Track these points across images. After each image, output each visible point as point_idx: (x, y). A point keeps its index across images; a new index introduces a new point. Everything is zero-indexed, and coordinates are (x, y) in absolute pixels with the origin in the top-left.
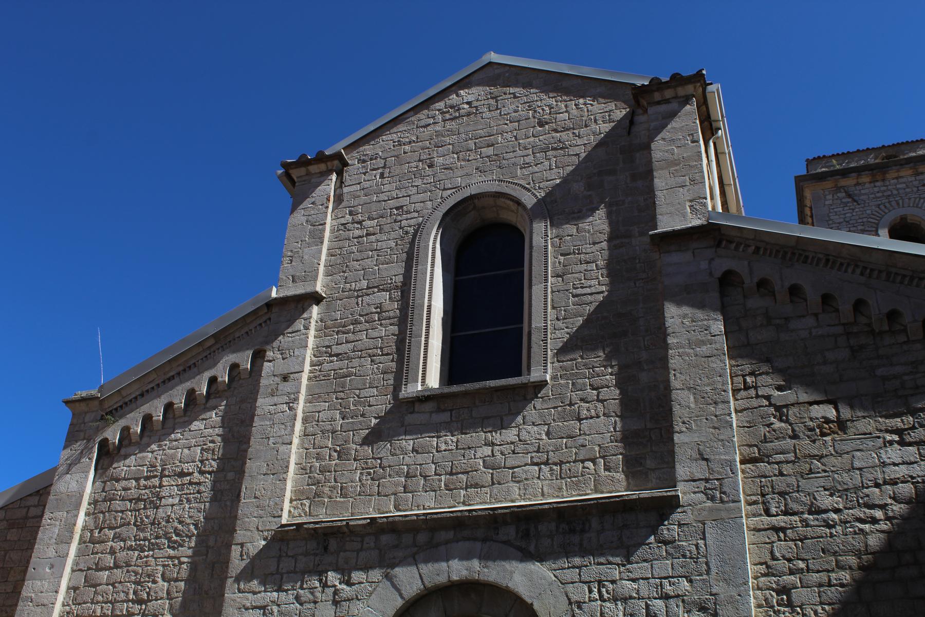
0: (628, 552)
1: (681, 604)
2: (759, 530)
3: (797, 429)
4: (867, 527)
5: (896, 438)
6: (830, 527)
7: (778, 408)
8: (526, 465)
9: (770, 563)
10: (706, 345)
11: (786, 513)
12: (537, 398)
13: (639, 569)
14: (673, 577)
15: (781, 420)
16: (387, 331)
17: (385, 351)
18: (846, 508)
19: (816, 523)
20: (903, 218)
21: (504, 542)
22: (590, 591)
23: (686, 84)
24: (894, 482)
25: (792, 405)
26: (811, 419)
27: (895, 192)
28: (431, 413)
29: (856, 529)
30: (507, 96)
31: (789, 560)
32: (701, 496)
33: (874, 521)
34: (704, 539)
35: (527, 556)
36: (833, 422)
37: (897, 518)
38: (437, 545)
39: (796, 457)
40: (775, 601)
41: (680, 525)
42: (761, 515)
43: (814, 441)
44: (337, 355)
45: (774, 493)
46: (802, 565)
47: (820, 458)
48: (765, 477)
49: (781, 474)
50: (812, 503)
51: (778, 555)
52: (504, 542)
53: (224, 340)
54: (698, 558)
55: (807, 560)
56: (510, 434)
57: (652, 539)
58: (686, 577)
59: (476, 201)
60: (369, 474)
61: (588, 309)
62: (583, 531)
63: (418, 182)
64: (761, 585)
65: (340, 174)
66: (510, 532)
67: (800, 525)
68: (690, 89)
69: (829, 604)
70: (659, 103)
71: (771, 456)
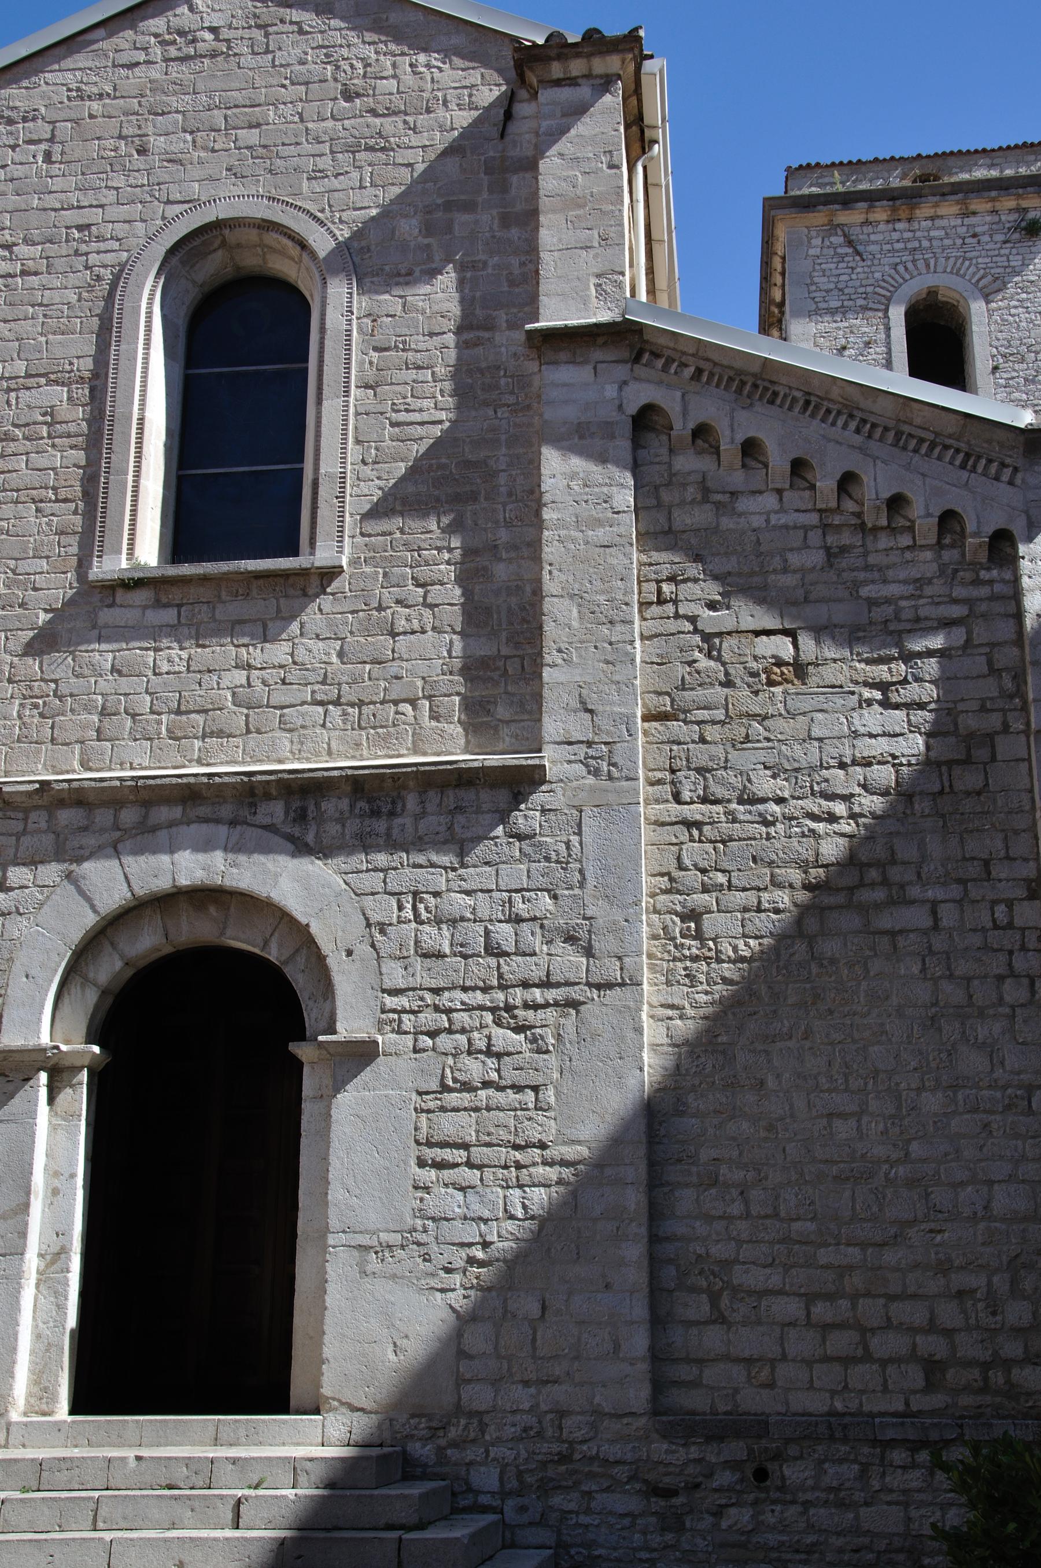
0: (462, 849)
1: (538, 930)
2: (663, 824)
3: (732, 671)
4: (820, 827)
5: (878, 695)
6: (766, 823)
7: (707, 637)
9: (676, 874)
10: (603, 526)
11: (704, 800)
12: (325, 593)
13: (477, 876)
14: (528, 890)
15: (709, 656)
18: (793, 797)
19: (748, 817)
20: (932, 292)
21: (265, 827)
22: (400, 908)
23: (609, 52)
25: (729, 633)
26: (755, 658)
27: (925, 244)
29: (806, 829)
31: (704, 871)
32: (580, 769)
33: (832, 818)
34: (579, 833)
35: (301, 848)
36: (788, 664)
39: (727, 715)
40: (677, 930)
41: (544, 811)
42: (667, 801)
43: (756, 693)
46: (721, 878)
49: (703, 740)
51: (687, 862)
52: (265, 827)
54: (568, 863)
56: (279, 652)
57: (500, 830)
58: (548, 891)
60: (36, 706)
62: (392, 814)
67: (723, 818)
69: (756, 937)
70: (558, 83)
71: (689, 711)
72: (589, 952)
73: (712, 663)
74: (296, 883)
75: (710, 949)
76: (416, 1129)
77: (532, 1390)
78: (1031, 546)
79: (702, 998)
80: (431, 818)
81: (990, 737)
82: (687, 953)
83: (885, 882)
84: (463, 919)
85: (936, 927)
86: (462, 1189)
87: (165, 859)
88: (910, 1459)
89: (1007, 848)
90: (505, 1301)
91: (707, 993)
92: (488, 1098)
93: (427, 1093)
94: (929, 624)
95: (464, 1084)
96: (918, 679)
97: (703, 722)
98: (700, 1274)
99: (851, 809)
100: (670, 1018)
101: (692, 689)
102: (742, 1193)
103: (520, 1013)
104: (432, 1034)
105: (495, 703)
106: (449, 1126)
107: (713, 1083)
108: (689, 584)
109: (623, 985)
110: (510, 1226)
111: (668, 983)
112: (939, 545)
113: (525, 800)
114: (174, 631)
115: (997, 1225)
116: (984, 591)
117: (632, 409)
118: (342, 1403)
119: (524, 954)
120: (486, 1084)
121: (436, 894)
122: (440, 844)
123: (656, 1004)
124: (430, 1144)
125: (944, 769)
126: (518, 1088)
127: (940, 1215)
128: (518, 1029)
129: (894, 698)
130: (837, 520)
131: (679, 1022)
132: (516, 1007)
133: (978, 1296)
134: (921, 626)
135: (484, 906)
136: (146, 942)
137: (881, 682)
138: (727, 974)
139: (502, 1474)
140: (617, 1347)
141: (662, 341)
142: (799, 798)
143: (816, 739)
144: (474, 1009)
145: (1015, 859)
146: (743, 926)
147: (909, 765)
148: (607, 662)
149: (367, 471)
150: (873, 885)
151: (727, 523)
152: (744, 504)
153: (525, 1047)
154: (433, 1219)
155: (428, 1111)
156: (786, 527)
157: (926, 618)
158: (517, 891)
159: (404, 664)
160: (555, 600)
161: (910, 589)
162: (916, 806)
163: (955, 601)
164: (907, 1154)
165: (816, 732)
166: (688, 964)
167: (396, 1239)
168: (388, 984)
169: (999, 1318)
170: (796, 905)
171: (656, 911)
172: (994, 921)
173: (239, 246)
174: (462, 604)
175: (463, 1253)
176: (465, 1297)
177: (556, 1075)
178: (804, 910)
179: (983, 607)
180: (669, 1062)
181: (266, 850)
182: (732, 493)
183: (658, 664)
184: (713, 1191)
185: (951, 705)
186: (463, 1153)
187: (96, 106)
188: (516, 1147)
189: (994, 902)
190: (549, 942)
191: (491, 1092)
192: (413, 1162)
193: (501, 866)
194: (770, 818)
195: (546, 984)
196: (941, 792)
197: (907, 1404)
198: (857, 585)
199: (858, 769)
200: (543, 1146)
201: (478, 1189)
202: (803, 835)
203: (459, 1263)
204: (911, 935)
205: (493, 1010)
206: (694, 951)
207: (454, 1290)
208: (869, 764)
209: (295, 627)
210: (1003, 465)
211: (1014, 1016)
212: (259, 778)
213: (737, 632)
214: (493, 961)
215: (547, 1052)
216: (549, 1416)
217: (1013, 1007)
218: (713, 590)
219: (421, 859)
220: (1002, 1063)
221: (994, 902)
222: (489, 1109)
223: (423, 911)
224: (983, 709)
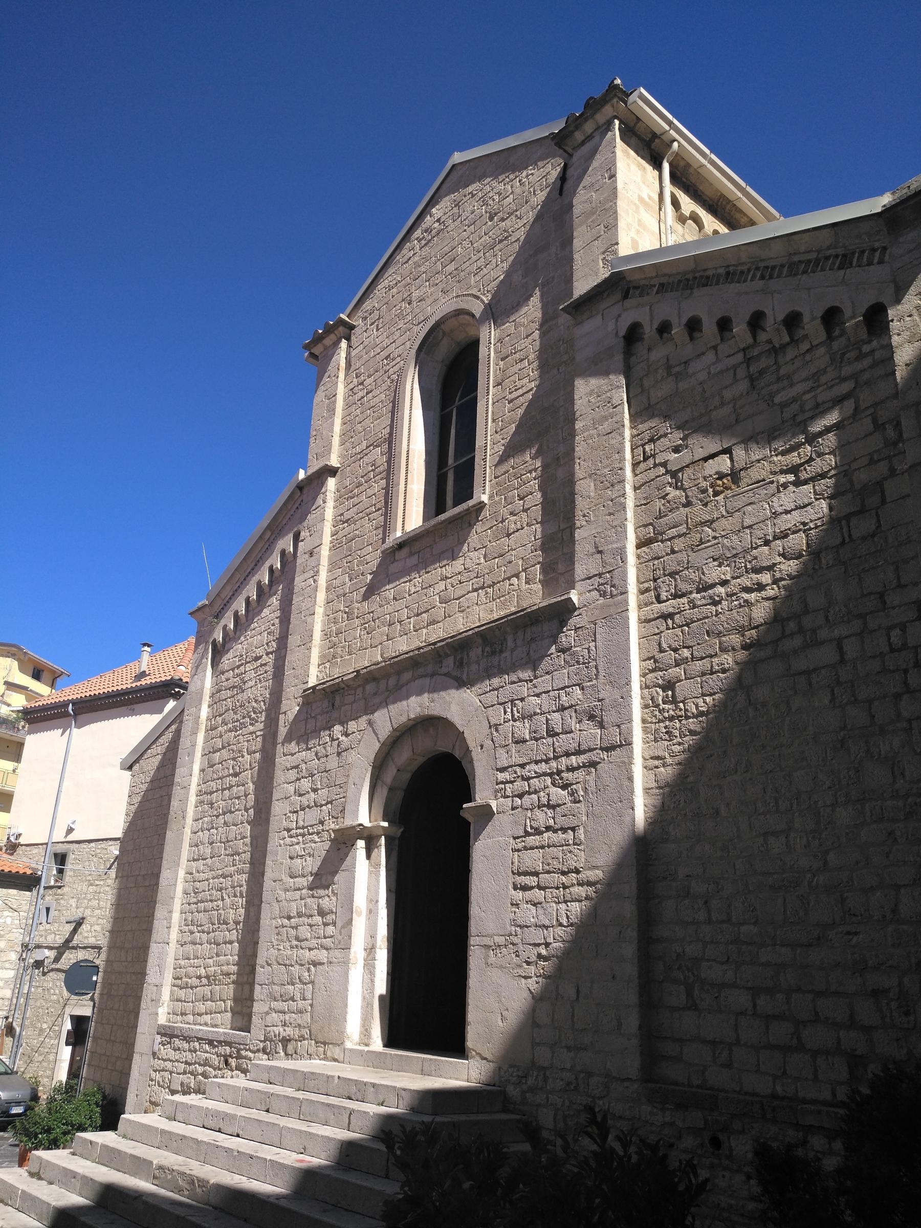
0: (534, 666)
1: (573, 714)
2: (649, 621)
3: (690, 494)
4: (752, 597)
5: (791, 478)
6: (715, 603)
7: (674, 474)
8: (469, 592)
9: (658, 656)
10: (607, 420)
11: (676, 596)
12: (478, 521)
13: (544, 683)
14: (568, 687)
15: (677, 488)
16: (377, 487)
17: (378, 506)
18: (733, 578)
19: (704, 602)
21: (445, 675)
22: (505, 713)
23: (602, 106)
24: (784, 535)
25: (687, 466)
26: (705, 478)
28: (405, 558)
29: (742, 601)
30: (468, 197)
31: (675, 650)
32: (595, 594)
33: (761, 587)
34: (595, 641)
35: (461, 683)
36: (727, 475)
37: (785, 579)
38: (402, 686)
39: (688, 528)
40: (660, 698)
41: (576, 629)
42: (652, 603)
43: (706, 505)
44: (347, 521)
45: (665, 575)
46: (686, 653)
47: (710, 523)
48: (658, 558)
49: (673, 552)
50: (700, 579)
51: (664, 645)
52: (445, 675)
53: (275, 529)
54: (589, 663)
55: (692, 647)
56: (458, 565)
57: (553, 649)
58: (578, 685)
59: (442, 326)
60: (365, 628)
61: (520, 412)
62: (501, 652)
63: (401, 324)
64: (648, 682)
65: (348, 339)
66: (449, 663)
67: (687, 607)
68: (608, 110)
69: (711, 695)
70: (583, 143)
71: (664, 533)
72: (602, 726)
73: (678, 492)
74: (461, 706)
75: (681, 710)
76: (512, 863)
77: (572, 1054)
78: (899, 307)
79: (675, 749)
80: (519, 649)
81: (880, 483)
82: (666, 715)
83: (801, 630)
84: (535, 714)
85: (842, 661)
86: (535, 905)
87: (404, 703)
88: (827, 1146)
89: (899, 578)
90: (557, 987)
91: (680, 744)
92: (549, 838)
93: (518, 838)
94: (826, 406)
95: (536, 829)
96: (820, 455)
97: (673, 538)
98: (678, 969)
99: (774, 575)
100: (657, 767)
101: (665, 516)
102: (706, 903)
103: (564, 775)
104: (520, 796)
105: (557, 563)
106: (534, 859)
107: (685, 815)
108: (662, 440)
109: (621, 746)
110: (559, 931)
111: (656, 740)
112: (830, 337)
113: (566, 625)
114: (417, 568)
115: (905, 927)
116: (867, 362)
117: (622, 332)
118: (478, 1054)
119: (567, 733)
120: (548, 828)
121: (522, 700)
122: (523, 666)
123: (648, 757)
124: (519, 874)
125: (844, 522)
126: (564, 830)
127: (854, 919)
128: (564, 787)
129: (803, 476)
130: (756, 352)
131: (662, 769)
132: (563, 771)
133: (891, 995)
134: (820, 410)
135: (546, 702)
136: (404, 756)
137: (793, 466)
138: (692, 727)
139: (555, 1115)
140: (620, 1025)
141: (637, 276)
142: (738, 577)
143: (747, 527)
144: (541, 775)
145: (906, 586)
146: (702, 687)
147: (816, 527)
148: (610, 514)
149: (498, 437)
150: (792, 634)
151: (683, 385)
152: (694, 367)
153: (568, 799)
154: (520, 926)
155: (518, 850)
156: (721, 372)
157: (824, 402)
158: (562, 689)
159: (513, 553)
160: (582, 481)
161: (810, 383)
162: (823, 561)
163: (844, 380)
164: (826, 863)
165: (748, 522)
166: (667, 723)
167: (501, 940)
168: (499, 765)
169: (912, 1018)
170: (737, 663)
171: (647, 687)
172: (890, 644)
173: (452, 331)
174: (541, 503)
175: (535, 951)
176: (537, 983)
177: (584, 818)
178: (744, 666)
179: (866, 376)
180: (657, 801)
181: (445, 688)
182: (685, 363)
183: (645, 504)
184: (686, 902)
185: (846, 468)
186: (536, 879)
187: (395, 290)
188: (564, 873)
189: (890, 628)
190: (580, 722)
191: (550, 834)
192: (511, 887)
193: (555, 673)
194: (717, 598)
195: (578, 752)
196: (843, 543)
197: (834, 1095)
198: (772, 396)
199: (777, 542)
200: (577, 871)
201: (544, 905)
202: (741, 606)
203: (533, 958)
204: (823, 672)
205: (551, 775)
206: (671, 712)
207: (531, 977)
208: (786, 536)
209: (465, 548)
210: (874, 250)
211: (911, 729)
212: (439, 644)
213: (693, 463)
214: (550, 740)
215: (579, 801)
216: (582, 1075)
217: (909, 721)
218: (676, 437)
219: (514, 677)
220: (903, 774)
221: (890, 628)
222: (549, 846)
223: (515, 712)
224: (872, 462)
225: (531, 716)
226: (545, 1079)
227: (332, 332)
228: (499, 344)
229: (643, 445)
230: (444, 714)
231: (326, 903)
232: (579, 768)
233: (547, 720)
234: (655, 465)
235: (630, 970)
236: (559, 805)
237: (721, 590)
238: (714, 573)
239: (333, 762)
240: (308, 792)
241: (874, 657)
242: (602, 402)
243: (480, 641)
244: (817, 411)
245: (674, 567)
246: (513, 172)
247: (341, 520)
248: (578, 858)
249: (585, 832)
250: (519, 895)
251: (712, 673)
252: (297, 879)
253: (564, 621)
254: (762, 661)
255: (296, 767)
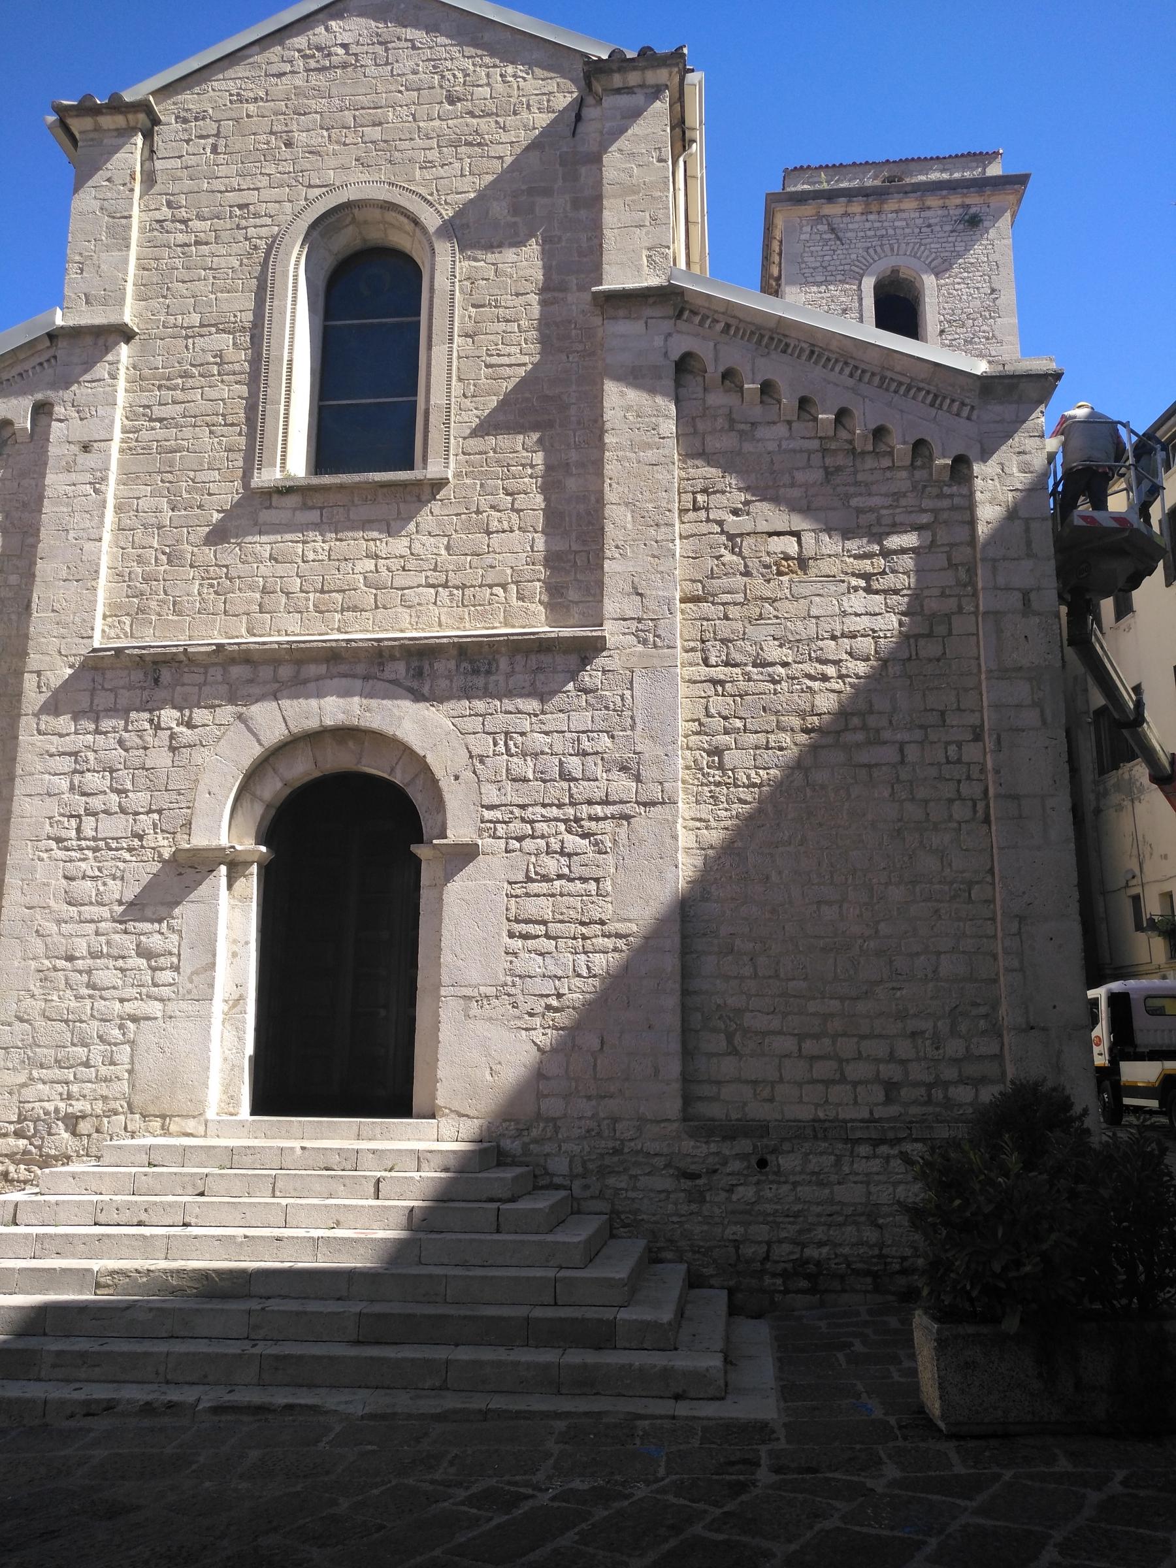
1: (600, 762)
2: (695, 682)
3: (750, 564)
4: (816, 685)
5: (862, 583)
6: (774, 682)
7: (731, 537)
8: (419, 586)
9: (704, 720)
11: (727, 664)
12: (435, 499)
13: (554, 721)
14: (592, 732)
15: (733, 553)
18: (795, 662)
19: (761, 677)
22: (495, 744)
23: (659, 66)
24: (853, 636)
25: (748, 534)
28: (295, 509)
31: (725, 718)
33: (825, 678)
34: (631, 689)
36: (793, 558)
41: (604, 672)
43: (768, 581)
44: (160, 420)
45: (716, 640)
46: (739, 724)
49: (726, 618)
51: (713, 711)
52: (390, 682)
56: (399, 545)
57: (570, 686)
58: (607, 732)
60: (212, 586)
67: (741, 678)
70: (618, 91)
71: (716, 595)
72: (638, 779)
73: (735, 558)
74: (420, 725)
82: (711, 779)
83: (864, 727)
85: (902, 762)
86: (541, 954)
87: (313, 702)
90: (574, 1038)
93: (516, 883)
97: (726, 603)
104: (520, 839)
113: (590, 663)
119: (589, 780)
121: (522, 734)
124: (517, 921)
126: (584, 880)
128: (584, 836)
134: (896, 528)
137: (865, 573)
140: (657, 1071)
141: (699, 302)
142: (800, 663)
144: (551, 820)
148: (654, 556)
150: (855, 729)
151: (748, 447)
156: (794, 451)
157: (901, 524)
158: (583, 732)
164: (877, 932)
166: (713, 788)
167: (491, 991)
169: (941, 1051)
172: (947, 757)
173: (366, 222)
177: (612, 870)
179: (945, 516)
182: (753, 424)
185: (918, 592)
186: (543, 928)
188: (582, 924)
189: (948, 743)
191: (563, 882)
192: (505, 934)
195: (606, 802)
196: (910, 659)
197: (871, 1113)
198: (848, 497)
200: (602, 923)
202: (803, 691)
204: (884, 768)
206: (717, 778)
208: (855, 637)
212: (386, 643)
215: (606, 853)
217: (959, 823)
220: (950, 865)
221: (948, 743)
222: (562, 895)
225: (536, 754)
226: (557, 1130)
227: (121, 113)
228: (467, 283)
229: (694, 493)
230: (389, 729)
231: (155, 942)
232: (605, 818)
233: (561, 763)
234: (708, 520)
235: (672, 1020)
236: (577, 854)
237: (781, 670)
238: (774, 652)
239: (160, 758)
240: (105, 793)
241: (932, 764)
242: (637, 422)
243: (455, 652)
244: (893, 530)
245: (726, 634)
246: (491, 56)
247: (140, 414)
248: (605, 909)
249: (614, 884)
250: (518, 944)
251: (767, 748)
252: (82, 908)
253: (586, 657)
254: (823, 747)
255: (75, 754)
